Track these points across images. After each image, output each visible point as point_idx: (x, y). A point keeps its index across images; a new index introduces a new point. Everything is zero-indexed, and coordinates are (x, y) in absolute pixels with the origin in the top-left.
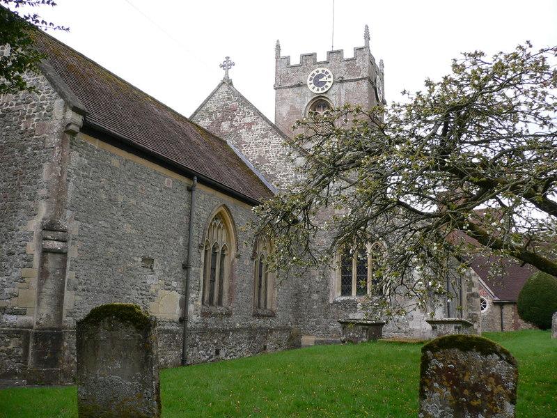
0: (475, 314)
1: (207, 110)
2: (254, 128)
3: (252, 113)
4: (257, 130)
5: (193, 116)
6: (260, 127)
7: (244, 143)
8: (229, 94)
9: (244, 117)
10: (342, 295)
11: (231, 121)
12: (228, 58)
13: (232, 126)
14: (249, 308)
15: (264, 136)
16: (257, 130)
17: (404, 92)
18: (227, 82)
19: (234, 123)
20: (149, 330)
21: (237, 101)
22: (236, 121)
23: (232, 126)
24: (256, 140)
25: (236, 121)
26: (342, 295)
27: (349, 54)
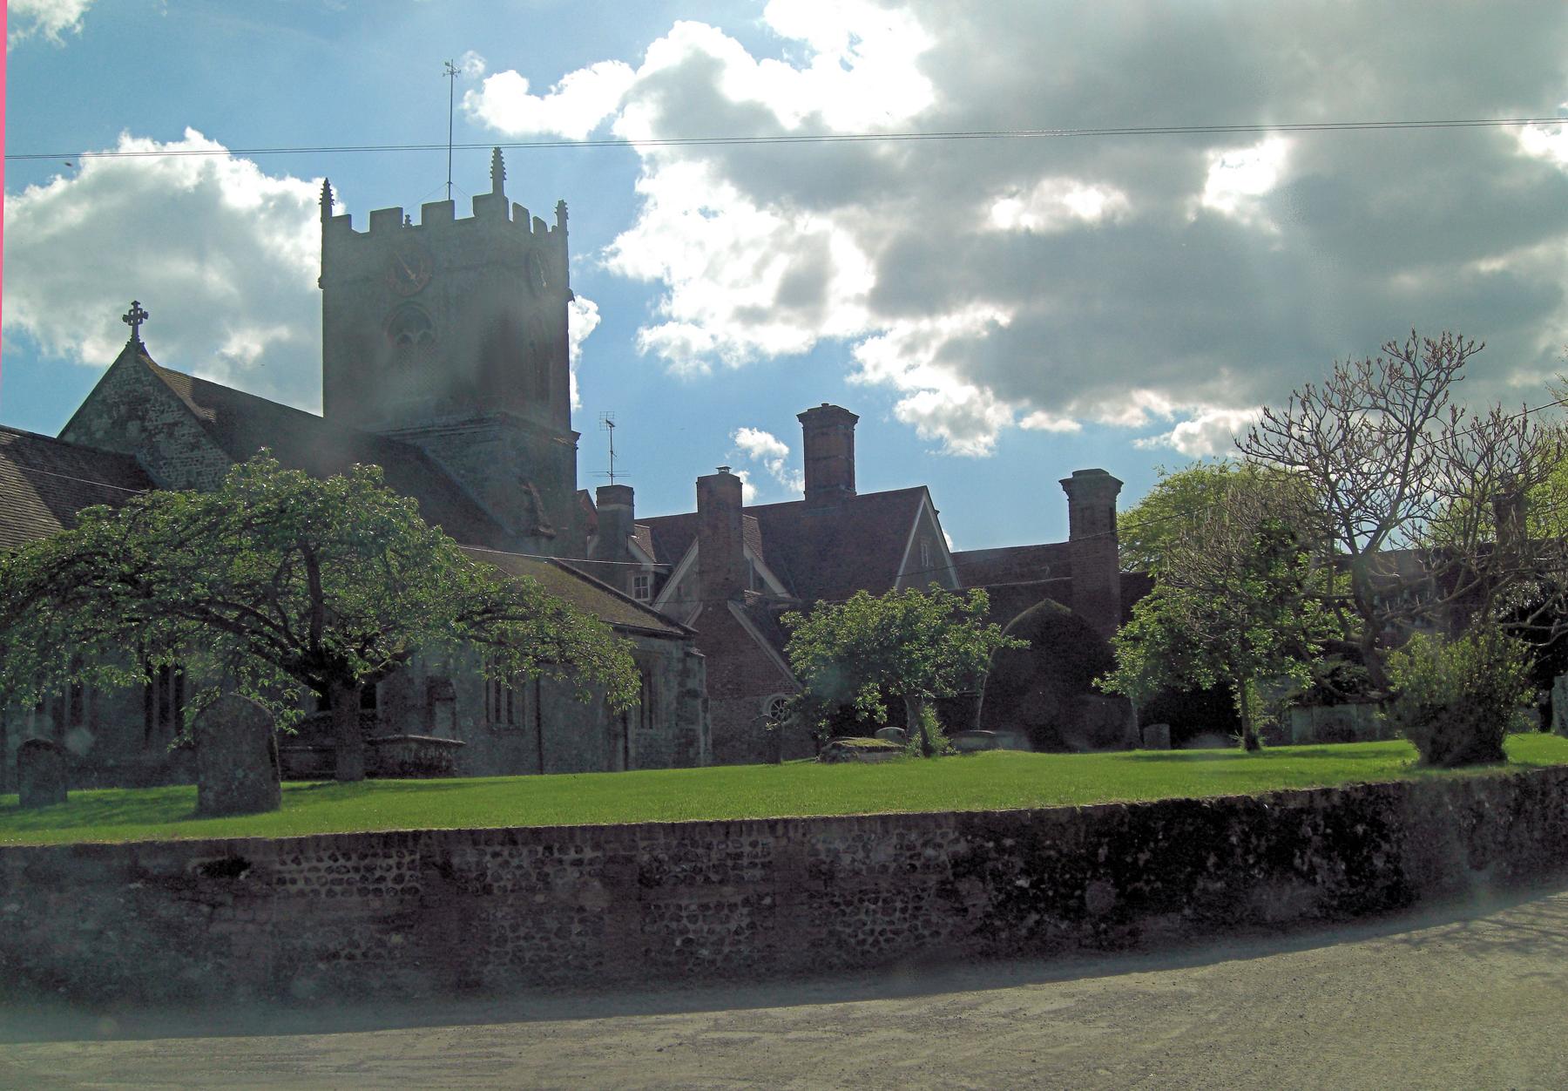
0: (691, 730)
1: (104, 400)
2: (178, 432)
3: (174, 404)
4: (183, 435)
5: (63, 433)
6: (187, 431)
7: (164, 458)
8: (137, 372)
9: (163, 412)
10: (319, 710)
11: (142, 419)
12: (135, 304)
13: (144, 429)
14: (1513, 621)
15: (194, 447)
16: (183, 435)
17: (686, 213)
18: (135, 349)
19: (146, 424)
20: (1463, 629)
21: (150, 385)
22: (151, 420)
23: (144, 429)
24: (181, 453)
25: (151, 420)
26: (319, 710)
27: (464, 211)
